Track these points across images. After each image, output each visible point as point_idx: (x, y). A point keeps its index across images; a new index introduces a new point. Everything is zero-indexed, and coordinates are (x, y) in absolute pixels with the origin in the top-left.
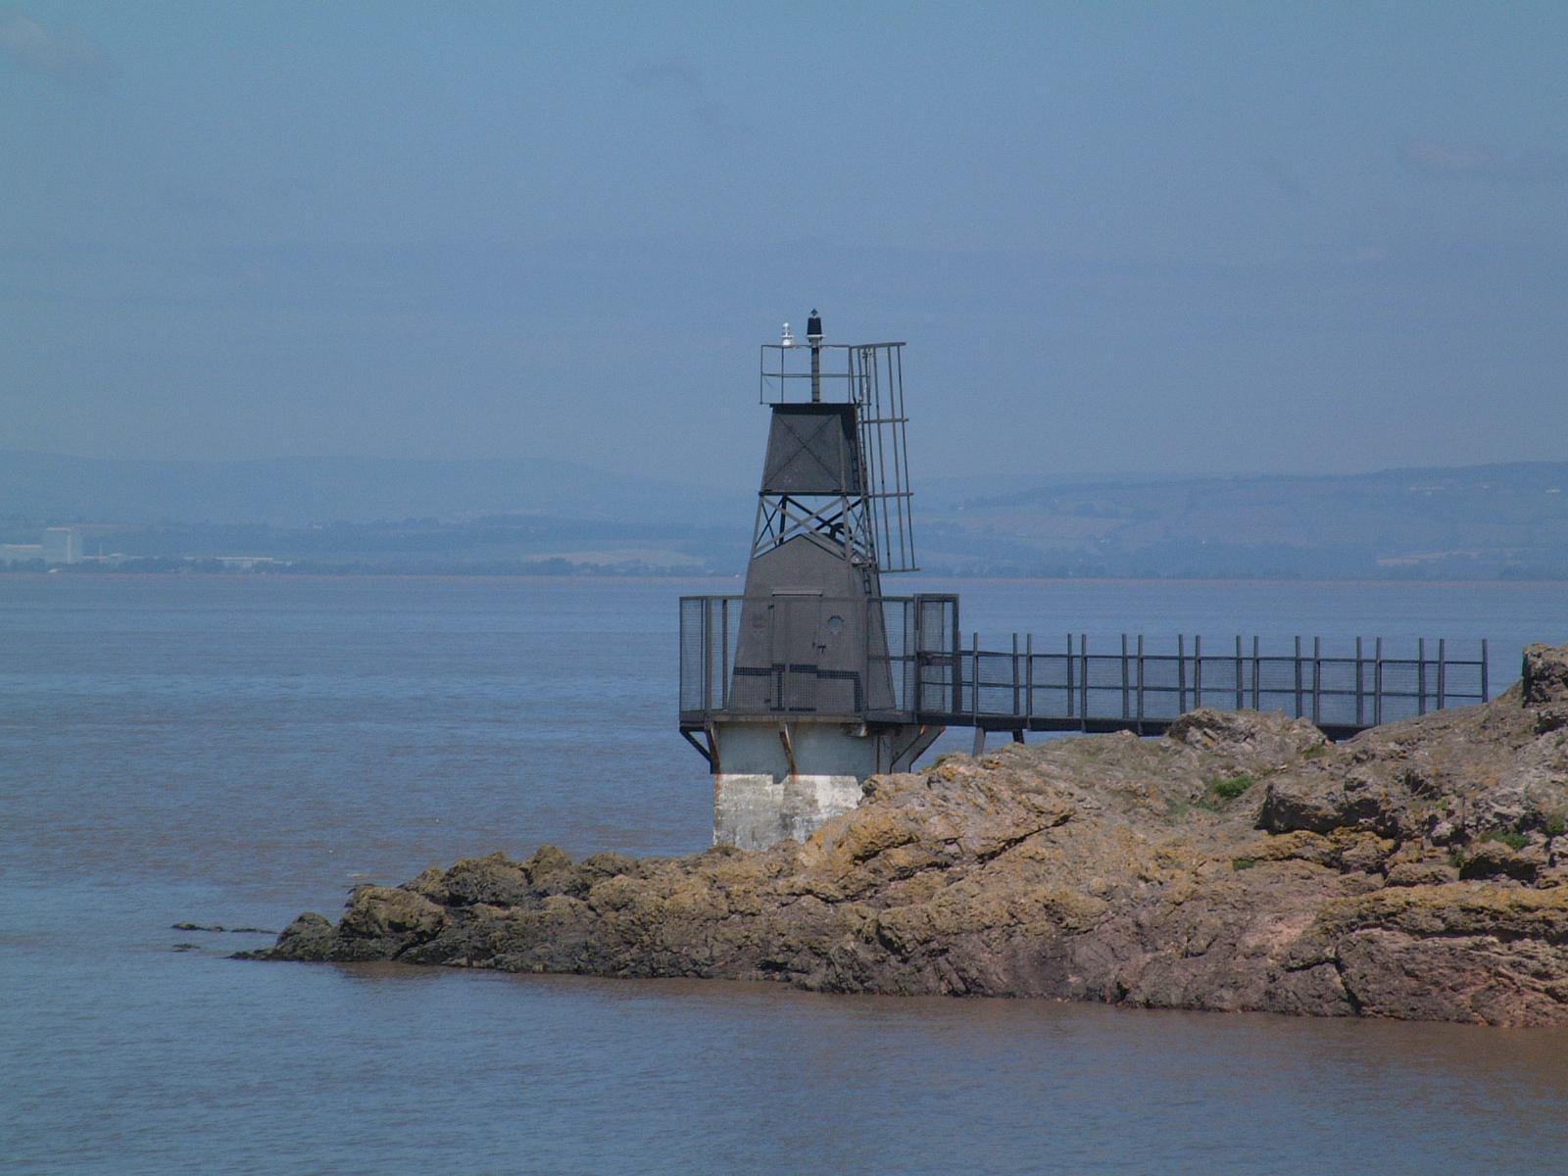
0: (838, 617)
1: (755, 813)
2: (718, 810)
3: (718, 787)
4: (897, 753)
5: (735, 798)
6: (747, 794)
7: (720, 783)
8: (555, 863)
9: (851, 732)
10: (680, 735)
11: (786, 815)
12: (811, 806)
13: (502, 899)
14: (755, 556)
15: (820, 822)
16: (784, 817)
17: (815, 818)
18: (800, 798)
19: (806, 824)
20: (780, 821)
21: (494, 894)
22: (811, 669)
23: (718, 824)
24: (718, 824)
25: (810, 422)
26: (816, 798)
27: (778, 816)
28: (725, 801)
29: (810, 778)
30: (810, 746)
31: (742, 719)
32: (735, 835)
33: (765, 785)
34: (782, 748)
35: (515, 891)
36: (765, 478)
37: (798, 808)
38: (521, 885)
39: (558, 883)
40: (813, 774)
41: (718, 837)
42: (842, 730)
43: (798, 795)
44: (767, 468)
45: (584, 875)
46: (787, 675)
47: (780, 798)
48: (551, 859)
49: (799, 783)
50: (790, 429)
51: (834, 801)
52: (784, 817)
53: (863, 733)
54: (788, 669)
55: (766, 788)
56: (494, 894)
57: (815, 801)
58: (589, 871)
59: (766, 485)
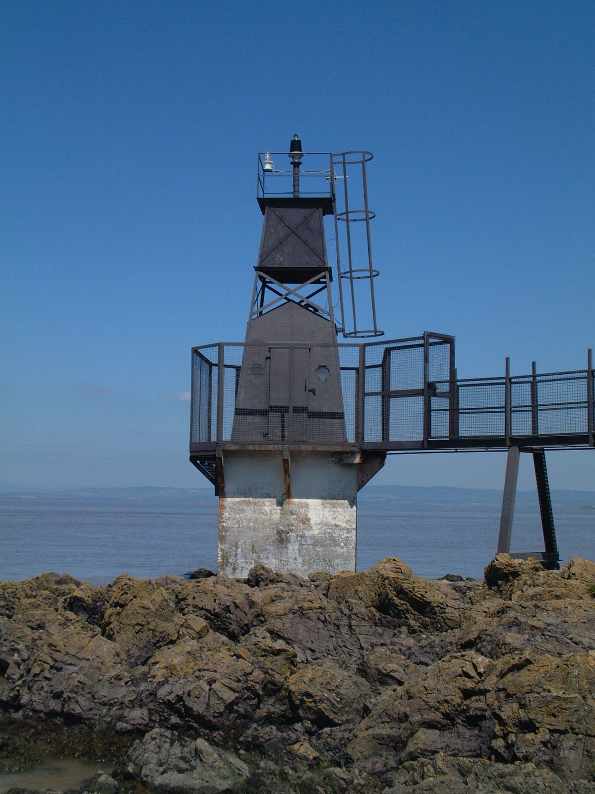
0: (325, 367)
1: (255, 529)
2: (223, 526)
3: (222, 507)
4: (363, 481)
5: (238, 516)
6: (250, 515)
7: (225, 504)
8: (153, 609)
9: (342, 460)
10: (190, 463)
11: (282, 531)
12: (304, 523)
13: (78, 710)
14: (253, 318)
15: (313, 537)
16: (280, 532)
17: (307, 533)
18: (295, 516)
19: (299, 539)
20: (277, 537)
21: (58, 696)
22: (303, 410)
23: (222, 539)
24: (222, 539)
25: (294, 215)
26: (309, 516)
27: (275, 532)
28: (229, 519)
29: (304, 500)
30: (307, 473)
31: (250, 448)
32: (237, 548)
33: (264, 506)
34: (283, 471)
35: (104, 692)
36: (261, 256)
37: (293, 525)
38: (118, 678)
39: (210, 682)
40: (307, 497)
41: (222, 550)
42: (334, 459)
43: (292, 514)
44: (263, 247)
45: (268, 662)
46: (289, 416)
47: (277, 516)
48: (146, 602)
49: (293, 503)
50: (281, 219)
51: (324, 520)
52: (280, 532)
53: (357, 460)
54: (291, 410)
55: (265, 508)
56: (58, 696)
57: (308, 520)
58: (278, 652)
59: (261, 262)
